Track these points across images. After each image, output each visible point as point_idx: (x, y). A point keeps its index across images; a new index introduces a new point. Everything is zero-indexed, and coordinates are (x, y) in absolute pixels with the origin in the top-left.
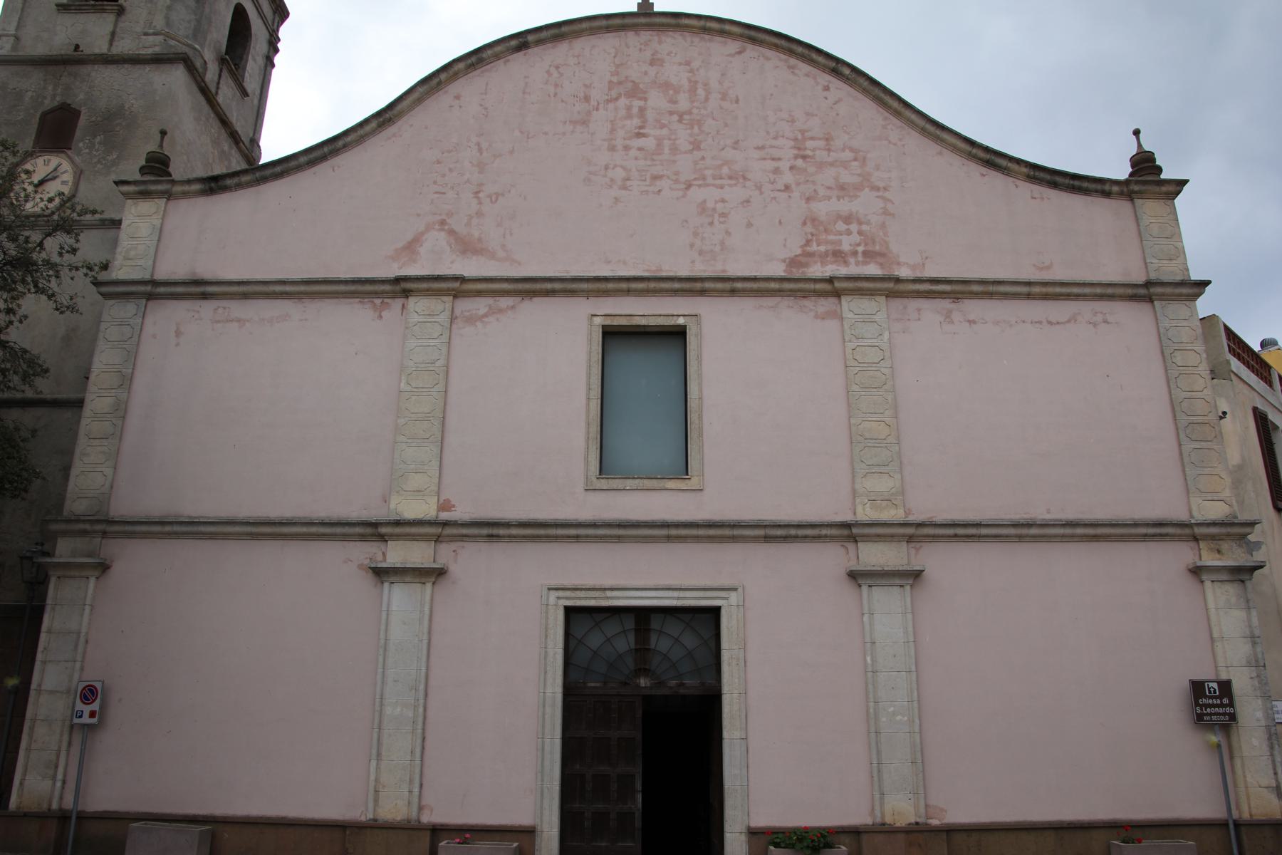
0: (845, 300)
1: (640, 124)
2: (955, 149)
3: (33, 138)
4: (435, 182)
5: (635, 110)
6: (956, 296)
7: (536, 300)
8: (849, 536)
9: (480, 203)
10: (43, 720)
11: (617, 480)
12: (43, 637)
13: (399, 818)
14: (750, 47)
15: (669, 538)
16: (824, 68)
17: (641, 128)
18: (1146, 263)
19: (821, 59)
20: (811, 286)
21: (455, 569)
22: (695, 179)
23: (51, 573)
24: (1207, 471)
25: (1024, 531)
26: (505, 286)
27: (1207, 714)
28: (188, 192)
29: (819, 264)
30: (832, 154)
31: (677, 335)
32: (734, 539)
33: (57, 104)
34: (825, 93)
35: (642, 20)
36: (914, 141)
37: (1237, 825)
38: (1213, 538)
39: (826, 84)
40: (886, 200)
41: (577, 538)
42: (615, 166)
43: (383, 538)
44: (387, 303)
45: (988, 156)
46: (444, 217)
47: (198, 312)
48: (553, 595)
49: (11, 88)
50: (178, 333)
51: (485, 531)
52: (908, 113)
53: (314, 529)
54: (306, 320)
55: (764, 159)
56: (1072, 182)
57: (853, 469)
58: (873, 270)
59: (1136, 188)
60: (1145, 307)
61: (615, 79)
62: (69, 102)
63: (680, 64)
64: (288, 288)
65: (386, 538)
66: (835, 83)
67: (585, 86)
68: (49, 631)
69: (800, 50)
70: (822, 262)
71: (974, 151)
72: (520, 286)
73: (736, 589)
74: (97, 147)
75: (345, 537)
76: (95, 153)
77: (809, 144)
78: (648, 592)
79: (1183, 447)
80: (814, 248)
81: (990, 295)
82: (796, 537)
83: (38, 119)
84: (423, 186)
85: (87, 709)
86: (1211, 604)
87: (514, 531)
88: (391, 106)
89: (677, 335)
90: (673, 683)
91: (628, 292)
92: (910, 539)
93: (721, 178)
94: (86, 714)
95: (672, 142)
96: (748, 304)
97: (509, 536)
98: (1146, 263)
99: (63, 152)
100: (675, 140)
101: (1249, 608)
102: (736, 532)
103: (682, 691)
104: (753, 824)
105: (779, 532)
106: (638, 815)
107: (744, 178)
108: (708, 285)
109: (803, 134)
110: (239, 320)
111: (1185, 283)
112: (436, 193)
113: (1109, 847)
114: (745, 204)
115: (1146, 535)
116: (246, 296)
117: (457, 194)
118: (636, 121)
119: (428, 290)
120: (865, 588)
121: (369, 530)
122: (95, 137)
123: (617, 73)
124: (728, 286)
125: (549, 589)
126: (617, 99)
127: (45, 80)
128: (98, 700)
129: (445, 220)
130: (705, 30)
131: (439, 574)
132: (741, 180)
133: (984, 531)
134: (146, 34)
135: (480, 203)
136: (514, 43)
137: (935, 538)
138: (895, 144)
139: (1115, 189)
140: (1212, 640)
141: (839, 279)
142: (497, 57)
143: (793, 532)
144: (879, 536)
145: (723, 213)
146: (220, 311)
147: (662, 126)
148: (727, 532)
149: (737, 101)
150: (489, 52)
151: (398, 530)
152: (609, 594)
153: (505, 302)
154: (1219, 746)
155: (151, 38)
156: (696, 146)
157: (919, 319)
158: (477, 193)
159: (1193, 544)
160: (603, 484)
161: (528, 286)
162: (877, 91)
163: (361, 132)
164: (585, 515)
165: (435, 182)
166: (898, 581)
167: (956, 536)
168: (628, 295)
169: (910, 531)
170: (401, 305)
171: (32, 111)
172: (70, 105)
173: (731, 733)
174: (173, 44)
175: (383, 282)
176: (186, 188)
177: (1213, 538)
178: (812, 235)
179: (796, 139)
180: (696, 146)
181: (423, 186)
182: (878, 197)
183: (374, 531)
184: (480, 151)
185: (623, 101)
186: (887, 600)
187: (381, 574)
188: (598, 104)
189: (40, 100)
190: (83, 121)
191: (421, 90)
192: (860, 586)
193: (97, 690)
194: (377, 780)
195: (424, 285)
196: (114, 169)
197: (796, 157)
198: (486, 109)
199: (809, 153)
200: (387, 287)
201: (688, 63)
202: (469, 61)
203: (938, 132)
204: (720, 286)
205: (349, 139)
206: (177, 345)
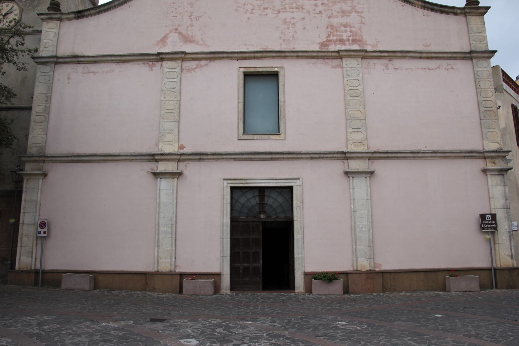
4: (172, 12)
6: (390, 58)
9: (192, 21)
10: (25, 235)
13: (167, 270)
15: (272, 159)
18: (470, 44)
20: (330, 54)
21: (186, 173)
22: (282, 9)
23: (24, 177)
24: (491, 130)
26: (203, 56)
27: (486, 227)
29: (333, 45)
31: (274, 75)
38: (492, 157)
40: (362, 17)
41: (235, 159)
42: (248, 4)
43: (156, 161)
46: (177, 27)
47: (76, 69)
48: (226, 182)
51: (198, 157)
53: (128, 158)
54: (121, 71)
56: (440, 9)
57: (347, 130)
58: (356, 47)
64: (113, 58)
68: (25, 201)
70: (335, 44)
72: (209, 56)
73: (299, 179)
75: (141, 161)
80: (331, 38)
81: (404, 58)
82: (323, 158)
84: (168, 14)
85: (42, 231)
86: (490, 184)
87: (209, 157)
89: (274, 75)
90: (274, 216)
91: (254, 58)
92: (369, 158)
93: (293, 8)
94: (42, 233)
96: (303, 62)
102: (299, 156)
103: (278, 220)
104: (306, 271)
106: (261, 268)
107: (302, 8)
108: (287, 54)
110: (93, 72)
112: (173, 16)
115: (465, 157)
116: (96, 62)
117: (182, 17)
119: (171, 58)
120: (351, 178)
121: (151, 158)
124: (295, 54)
125: (224, 180)
128: (47, 227)
129: (177, 28)
133: (399, 155)
135: (192, 21)
137: (379, 158)
139: (459, 11)
141: (342, 51)
143: (322, 156)
144: (357, 157)
145: (293, 24)
146: (86, 68)
148: (295, 156)
152: (248, 181)
153: (203, 63)
154: (490, 240)
158: (191, 16)
159: (484, 160)
160: (245, 137)
161: (213, 56)
164: (238, 150)
165: (172, 12)
166: (364, 175)
167: (388, 157)
169: (370, 155)
170: (160, 65)
173: (297, 236)
176: (68, 16)
177: (492, 157)
178: (331, 32)
181: (168, 14)
182: (358, 16)
183: (153, 158)
186: (360, 183)
187: (156, 175)
194: (158, 256)
195: (169, 56)
196: (37, 8)
200: (154, 57)
204: (292, 54)
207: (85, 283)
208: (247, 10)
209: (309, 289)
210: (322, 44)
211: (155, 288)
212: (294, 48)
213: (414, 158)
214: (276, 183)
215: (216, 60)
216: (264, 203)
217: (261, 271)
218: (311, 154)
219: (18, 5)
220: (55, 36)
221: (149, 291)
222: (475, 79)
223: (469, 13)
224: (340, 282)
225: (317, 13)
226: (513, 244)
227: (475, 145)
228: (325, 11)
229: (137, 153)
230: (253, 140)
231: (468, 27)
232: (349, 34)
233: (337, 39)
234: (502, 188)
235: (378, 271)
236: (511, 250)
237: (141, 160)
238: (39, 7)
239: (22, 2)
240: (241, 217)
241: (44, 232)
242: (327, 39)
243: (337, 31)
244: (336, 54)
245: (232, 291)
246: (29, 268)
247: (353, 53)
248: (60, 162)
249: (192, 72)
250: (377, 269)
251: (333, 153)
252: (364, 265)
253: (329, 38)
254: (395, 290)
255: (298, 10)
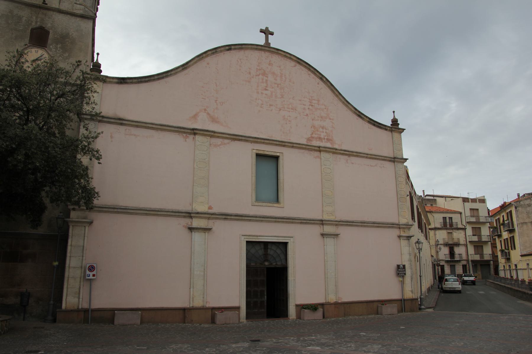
0: (322, 153)
1: (266, 86)
2: (351, 110)
3: (29, 39)
4: (202, 94)
5: (264, 81)
6: (349, 155)
7: (236, 141)
8: (321, 223)
9: (217, 105)
10: (72, 277)
11: (260, 203)
12: (69, 248)
13: (200, 306)
14: (298, 65)
15: (275, 222)
16: (318, 77)
17: (266, 87)
18: (394, 151)
19: (318, 74)
20: (314, 148)
21: (214, 229)
22: (282, 108)
23: (70, 224)
24: (403, 210)
25: (363, 224)
26: (227, 136)
27: (400, 273)
28: (112, 82)
29: (315, 141)
30: (319, 106)
31: (277, 158)
32: (292, 223)
33: (38, 26)
34: (318, 85)
35: (267, 49)
36: (340, 105)
37: (404, 300)
38: (403, 228)
39: (318, 82)
40: (333, 123)
41: (250, 220)
42: (259, 99)
43: (191, 217)
44: (188, 136)
45: (359, 114)
47: (119, 130)
48: (243, 237)
49: (16, 13)
50: (112, 137)
51: (224, 217)
52: (340, 96)
53: (169, 213)
55: (301, 104)
56: (379, 125)
57: (323, 204)
58: (328, 145)
59: (394, 129)
60: (393, 163)
61: (258, 68)
62: (44, 26)
63: (278, 67)
64: (154, 126)
65: (192, 217)
66: (321, 83)
67: (249, 68)
68: (71, 246)
69: (312, 69)
70: (316, 140)
71: (356, 112)
72: (232, 137)
73: (292, 237)
74: (59, 49)
76: (58, 52)
77: (314, 101)
78: (269, 237)
79: (399, 204)
80: (314, 135)
81: (357, 156)
82: (309, 223)
83: (30, 31)
85: (91, 274)
86: (402, 245)
87: (232, 217)
88: (187, 63)
89: (277, 158)
90: (274, 264)
91: (263, 143)
92: (336, 225)
93: (289, 109)
94: (91, 275)
95: (275, 94)
96: (296, 151)
97: (231, 219)
98: (394, 151)
99: (44, 49)
100: (276, 93)
101: (409, 246)
102: (294, 221)
103: (277, 266)
104: (297, 304)
105: (305, 221)
106: (265, 302)
107: (296, 110)
108: (286, 144)
109: (312, 98)
110: (135, 135)
111: (403, 159)
112: (202, 98)
113: (378, 307)
114: (296, 118)
115: (389, 227)
116: (137, 126)
117: (210, 100)
118: (265, 84)
119: (202, 134)
120: (325, 238)
121: (187, 215)
122: (57, 44)
123: (259, 66)
124: (292, 145)
125: (242, 235)
126: (259, 75)
127: (31, 14)
128: (95, 270)
129: (206, 109)
130: (285, 56)
131: (209, 230)
132: (295, 110)
133: (354, 224)
134: (76, 3)
135: (217, 105)
136: (227, 48)
137: (342, 225)
138: (336, 106)
139: (389, 129)
140: (401, 254)
141: (322, 147)
142: (221, 51)
143: (308, 222)
144: (329, 224)
145: (290, 121)
146: (127, 130)
147: (273, 88)
148: (291, 221)
149: (294, 83)
150: (219, 49)
151: (197, 215)
152: (259, 237)
153: (226, 141)
154: (402, 281)
155: (78, 6)
156: (282, 97)
157: (340, 161)
158: (216, 101)
159: (399, 229)
160: (257, 204)
161: (234, 137)
162: (332, 88)
163: (176, 71)
164: (251, 213)
165: (202, 94)
166: (333, 237)
167: (347, 225)
168: (263, 144)
169: (337, 223)
170: (193, 138)
171: (26, 27)
172: (44, 28)
173: (291, 278)
174: (87, 10)
175: (188, 129)
176: (112, 80)
177: (403, 228)
178: (314, 131)
179: (310, 99)
180: (282, 97)
182: (331, 122)
183: (189, 215)
184: (216, 85)
185: (261, 76)
186: (329, 241)
187: (191, 229)
188: (253, 76)
189: (30, 22)
190: (51, 36)
191: (197, 59)
192: (324, 237)
193: (95, 268)
194: (193, 295)
195: (202, 132)
196: (67, 60)
197: (310, 105)
198: (218, 70)
199: (313, 104)
200: (189, 131)
201: (280, 67)
202: (213, 52)
203: (347, 104)
204: (289, 145)
205: (172, 72)
206: (112, 141)
207: (136, 319)
208: (258, 104)
209: (299, 316)
210: (308, 140)
211: (192, 321)
212: (290, 140)
213: (362, 226)
214: (278, 239)
215: (236, 140)
216: (268, 254)
217: (265, 304)
218: (302, 220)
219: (48, 53)
220: (98, 96)
221: (188, 323)
222: (396, 175)
223: (394, 131)
224: (321, 310)
225: (305, 115)
226: (413, 284)
227: (394, 219)
228: (310, 114)
229: (176, 211)
230: (262, 207)
231: (393, 140)
232: (325, 134)
233: (317, 137)
234: (408, 248)
235: (340, 302)
236: (412, 287)
237: (179, 216)
238: (70, 60)
239: (52, 51)
240: (252, 264)
241: (93, 274)
242: (311, 136)
243: (317, 131)
244: (317, 149)
245: (247, 320)
246: (76, 308)
247: (328, 150)
248: (106, 212)
249: (218, 147)
250: (340, 301)
251: (315, 220)
252: (332, 298)
253: (312, 136)
254: (350, 315)
255: (292, 110)
